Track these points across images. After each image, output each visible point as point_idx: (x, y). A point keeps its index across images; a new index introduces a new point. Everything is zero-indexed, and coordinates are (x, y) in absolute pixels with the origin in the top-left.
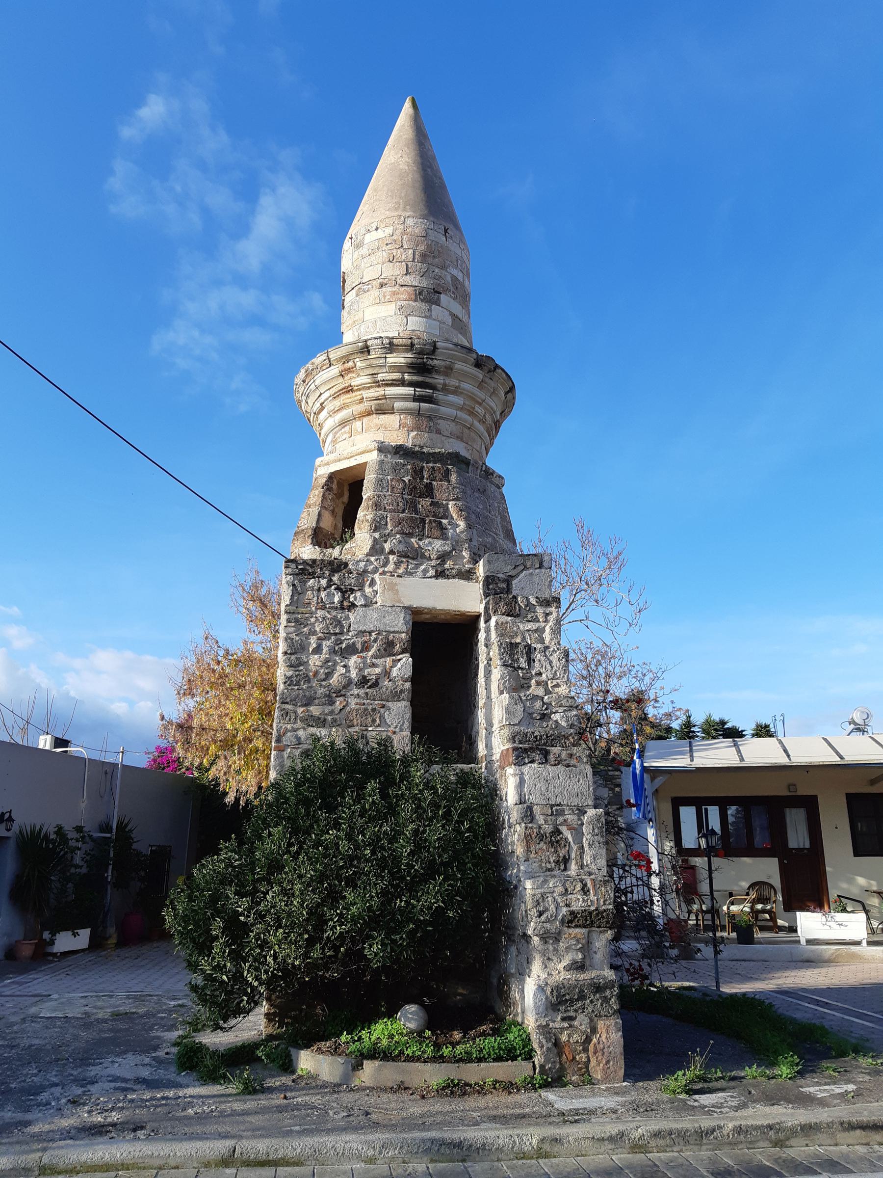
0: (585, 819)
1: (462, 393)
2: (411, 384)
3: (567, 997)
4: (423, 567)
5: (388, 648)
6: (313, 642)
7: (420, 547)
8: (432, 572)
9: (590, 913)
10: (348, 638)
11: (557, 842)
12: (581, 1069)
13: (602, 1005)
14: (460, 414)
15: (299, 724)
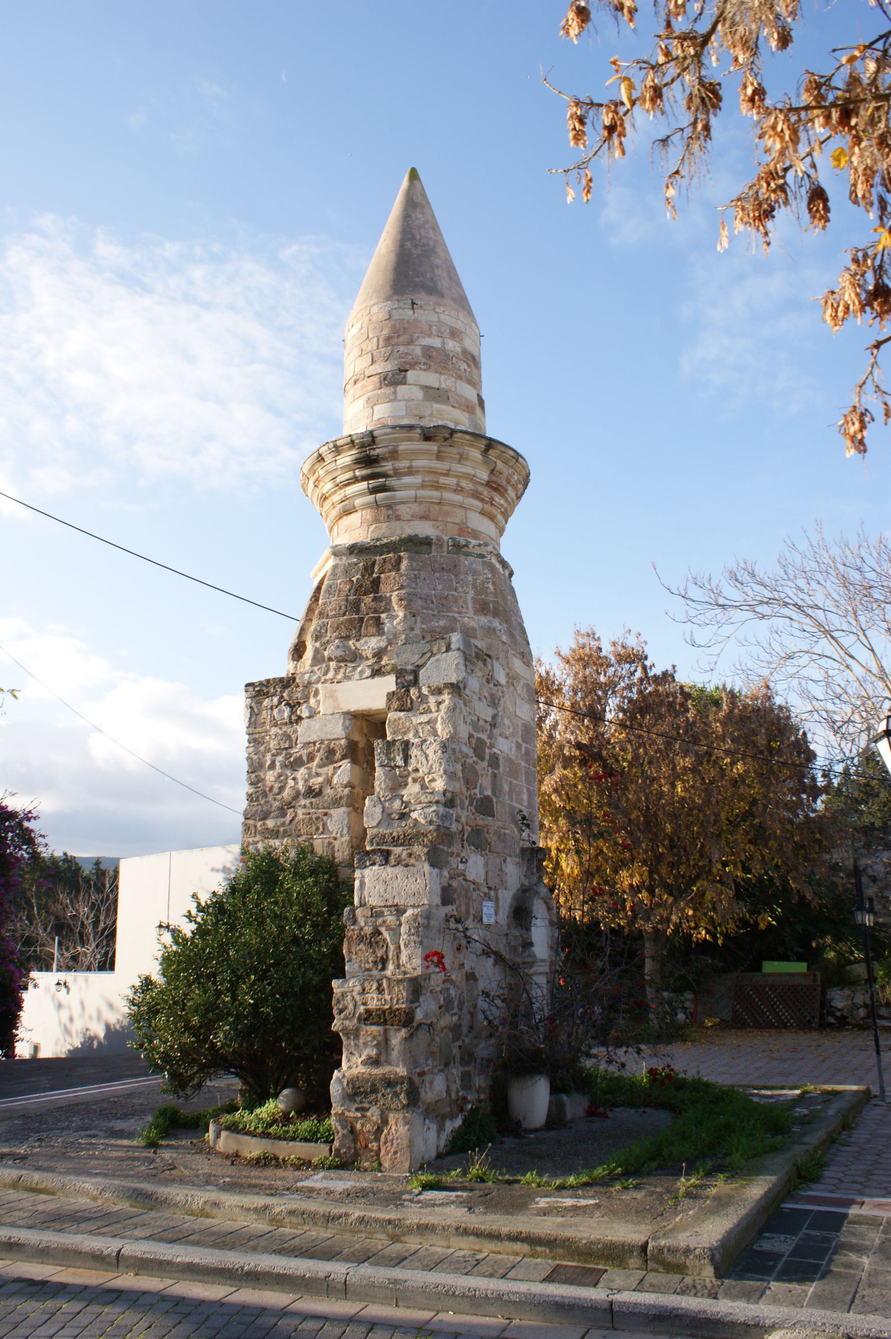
0: (403, 919)
1: (418, 471)
2: (365, 478)
3: (362, 1089)
4: (359, 669)
5: (330, 756)
6: (268, 759)
7: (356, 648)
8: (368, 672)
9: (384, 1012)
10: (298, 751)
11: (377, 943)
12: (372, 1157)
13: (392, 1099)
14: (421, 493)
15: (258, 838)
